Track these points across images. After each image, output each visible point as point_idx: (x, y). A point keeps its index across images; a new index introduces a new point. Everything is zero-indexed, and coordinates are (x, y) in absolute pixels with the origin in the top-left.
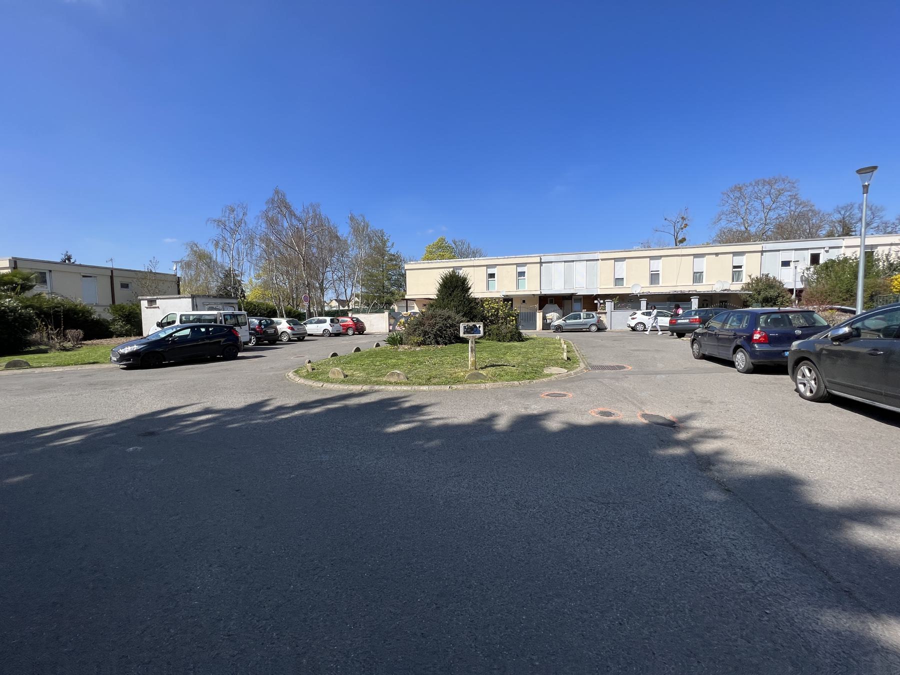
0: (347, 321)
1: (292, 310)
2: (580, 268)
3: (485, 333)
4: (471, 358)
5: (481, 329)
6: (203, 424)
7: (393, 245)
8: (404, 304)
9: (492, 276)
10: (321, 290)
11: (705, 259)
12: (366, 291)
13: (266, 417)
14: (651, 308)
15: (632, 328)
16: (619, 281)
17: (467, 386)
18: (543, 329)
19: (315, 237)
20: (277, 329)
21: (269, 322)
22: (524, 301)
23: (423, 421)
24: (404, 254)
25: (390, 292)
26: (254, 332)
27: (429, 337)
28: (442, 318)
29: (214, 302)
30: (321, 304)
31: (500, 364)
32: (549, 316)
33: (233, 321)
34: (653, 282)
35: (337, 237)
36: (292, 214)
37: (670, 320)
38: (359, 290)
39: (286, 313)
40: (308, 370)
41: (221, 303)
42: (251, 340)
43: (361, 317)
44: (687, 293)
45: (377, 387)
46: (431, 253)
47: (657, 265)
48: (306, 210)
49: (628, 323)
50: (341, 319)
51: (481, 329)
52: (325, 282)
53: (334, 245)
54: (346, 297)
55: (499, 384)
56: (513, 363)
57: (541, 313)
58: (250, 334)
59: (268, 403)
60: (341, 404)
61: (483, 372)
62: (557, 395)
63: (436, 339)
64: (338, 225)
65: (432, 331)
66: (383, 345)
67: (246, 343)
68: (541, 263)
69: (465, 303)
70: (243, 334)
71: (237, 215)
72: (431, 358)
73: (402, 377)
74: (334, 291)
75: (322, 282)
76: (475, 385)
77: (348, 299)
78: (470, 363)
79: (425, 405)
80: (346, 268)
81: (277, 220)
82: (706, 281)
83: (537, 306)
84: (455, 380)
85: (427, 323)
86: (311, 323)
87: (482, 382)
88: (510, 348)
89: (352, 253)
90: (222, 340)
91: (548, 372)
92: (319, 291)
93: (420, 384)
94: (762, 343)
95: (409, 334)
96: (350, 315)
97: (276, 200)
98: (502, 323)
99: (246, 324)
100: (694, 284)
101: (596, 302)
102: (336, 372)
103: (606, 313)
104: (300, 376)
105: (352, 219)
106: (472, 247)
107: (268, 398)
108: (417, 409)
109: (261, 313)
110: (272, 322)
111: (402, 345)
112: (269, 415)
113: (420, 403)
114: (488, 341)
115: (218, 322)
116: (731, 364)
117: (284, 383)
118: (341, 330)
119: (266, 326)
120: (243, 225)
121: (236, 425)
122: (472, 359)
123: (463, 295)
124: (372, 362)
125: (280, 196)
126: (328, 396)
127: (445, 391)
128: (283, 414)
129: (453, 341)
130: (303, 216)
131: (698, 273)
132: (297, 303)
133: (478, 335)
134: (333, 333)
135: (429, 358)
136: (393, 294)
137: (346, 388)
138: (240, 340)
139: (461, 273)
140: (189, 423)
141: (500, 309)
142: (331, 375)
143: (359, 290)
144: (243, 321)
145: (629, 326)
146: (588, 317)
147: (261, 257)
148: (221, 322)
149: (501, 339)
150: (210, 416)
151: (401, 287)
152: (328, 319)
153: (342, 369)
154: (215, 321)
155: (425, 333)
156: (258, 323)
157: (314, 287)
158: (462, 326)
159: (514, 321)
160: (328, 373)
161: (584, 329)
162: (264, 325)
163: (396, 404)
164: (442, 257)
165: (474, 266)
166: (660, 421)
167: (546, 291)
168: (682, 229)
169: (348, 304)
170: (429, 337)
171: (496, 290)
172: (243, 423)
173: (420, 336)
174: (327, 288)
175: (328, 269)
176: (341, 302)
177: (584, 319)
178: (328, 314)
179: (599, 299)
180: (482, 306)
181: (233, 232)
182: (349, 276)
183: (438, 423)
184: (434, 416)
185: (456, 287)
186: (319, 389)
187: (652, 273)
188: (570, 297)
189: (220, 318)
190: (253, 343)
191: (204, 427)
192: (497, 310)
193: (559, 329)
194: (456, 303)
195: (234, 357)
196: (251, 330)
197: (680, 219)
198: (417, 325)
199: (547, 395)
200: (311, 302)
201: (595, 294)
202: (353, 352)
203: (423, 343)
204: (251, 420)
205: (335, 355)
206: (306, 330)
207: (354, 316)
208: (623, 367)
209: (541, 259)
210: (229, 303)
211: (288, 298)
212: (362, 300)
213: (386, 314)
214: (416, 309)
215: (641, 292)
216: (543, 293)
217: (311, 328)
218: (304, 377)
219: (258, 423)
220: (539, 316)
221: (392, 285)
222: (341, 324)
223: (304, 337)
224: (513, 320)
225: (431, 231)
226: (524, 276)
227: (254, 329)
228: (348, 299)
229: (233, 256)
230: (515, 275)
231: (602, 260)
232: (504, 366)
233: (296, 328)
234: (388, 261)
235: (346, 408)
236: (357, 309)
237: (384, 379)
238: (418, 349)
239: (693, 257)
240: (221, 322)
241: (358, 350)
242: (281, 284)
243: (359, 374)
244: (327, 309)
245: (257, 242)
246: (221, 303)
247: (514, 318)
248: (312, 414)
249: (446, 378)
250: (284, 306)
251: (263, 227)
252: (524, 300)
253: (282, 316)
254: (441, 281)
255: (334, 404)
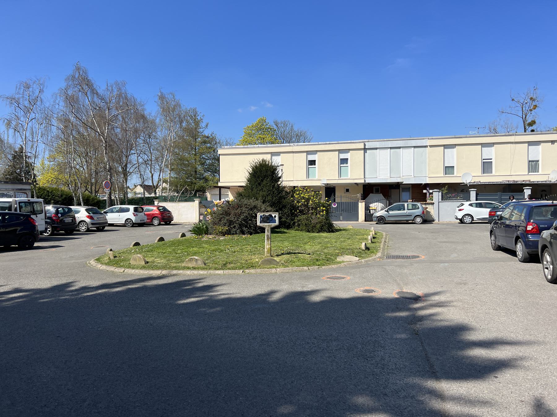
0: (152, 210)
1: (90, 197)
2: (407, 155)
3: (280, 222)
4: (267, 246)
5: (276, 219)
6: (16, 299)
7: (207, 126)
8: (217, 191)
9: (312, 163)
10: (124, 175)
11: (540, 146)
12: (175, 176)
13: (72, 295)
14: (510, 199)
15: (460, 220)
16: (449, 170)
17: (259, 271)
18: (365, 221)
19: (120, 117)
20: (75, 218)
21: (67, 211)
22: (347, 190)
23: (211, 296)
24: (220, 136)
25: (204, 178)
26: (50, 221)
27: (234, 227)
28: (248, 208)
29: (5, 188)
30: (124, 190)
31: (297, 252)
32: (373, 206)
33: (29, 208)
34: (486, 170)
35: (143, 117)
36: (94, 92)
37: (490, 212)
38: (167, 175)
39: (83, 200)
40: (109, 258)
41: (13, 190)
42: (46, 229)
43: (169, 206)
44: (520, 183)
45: (175, 272)
46: (250, 135)
47: (490, 153)
48: (110, 88)
49: (456, 214)
50: (146, 207)
51: (277, 219)
52: (129, 166)
53: (140, 125)
54: (153, 183)
55: (290, 269)
56: (309, 251)
57: (364, 203)
58: (46, 222)
59: (73, 284)
60: (141, 285)
61: (277, 259)
62: (336, 278)
63: (241, 228)
64: (145, 102)
65: (238, 220)
66: (189, 235)
67: (42, 233)
68: (365, 149)
69: (273, 193)
70: (40, 222)
71: (33, 92)
72: (232, 246)
73: (199, 262)
74: (139, 176)
75: (126, 165)
76: (266, 269)
77: (155, 184)
78: (266, 250)
79: (217, 285)
80: (153, 150)
81: (78, 99)
82: (542, 171)
83: (359, 195)
84: (249, 266)
85: (233, 212)
86: (112, 212)
87: (274, 267)
88: (313, 238)
89: (160, 134)
90: (19, 228)
91: (340, 260)
92: (122, 176)
93: (216, 269)
94: (534, 234)
95: (215, 224)
96: (156, 203)
97: (77, 76)
98: (312, 213)
99: (43, 212)
100: (530, 174)
101: (425, 191)
102: (137, 258)
103: (433, 203)
104: (102, 264)
105: (162, 97)
106: (295, 129)
107: (72, 281)
108: (209, 288)
109: (55, 200)
110: (70, 210)
111: (208, 234)
112: (75, 293)
113: (213, 283)
114: (297, 232)
115: (13, 209)
116: (513, 253)
117: (86, 269)
118: (146, 220)
119: (63, 214)
120: (38, 103)
121: (46, 300)
122: (268, 247)
123: (273, 184)
124: (174, 250)
125: (81, 72)
126: (129, 279)
127: (238, 275)
128: (88, 292)
129: (258, 231)
130: (107, 95)
131: (533, 161)
132: (95, 188)
133: (273, 225)
134: (137, 222)
135: (230, 247)
136: (206, 180)
137: (146, 272)
138: (36, 229)
139: (276, 161)
140: (3, 299)
141: (311, 198)
142: (132, 262)
143: (167, 175)
144: (39, 208)
145: (457, 219)
146: (415, 207)
147: (58, 137)
148: (16, 210)
149: (310, 230)
150: (21, 294)
151: (216, 173)
152: (132, 207)
153: (144, 256)
154: (10, 208)
155: (231, 222)
156: (54, 211)
157: (116, 171)
158: (259, 215)
159: (324, 211)
160: (129, 260)
161: (410, 220)
162: (61, 213)
163: (189, 285)
164: (263, 142)
165: (293, 152)
166: (409, 296)
167: (371, 179)
168: (531, 110)
169: (155, 191)
170: (234, 227)
171: (317, 178)
172: (53, 299)
173: (225, 225)
174: (131, 173)
175: (133, 152)
176: (147, 188)
177: (408, 209)
178: (131, 202)
179: (428, 189)
180: (293, 196)
181: (27, 111)
182: (157, 159)
183: (223, 297)
184: (221, 293)
185: (265, 176)
186: (120, 274)
187: (484, 161)
188: (397, 186)
189: (15, 206)
190: (48, 233)
191: (18, 302)
192: (308, 200)
193: (381, 220)
194: (264, 193)
195: (31, 247)
196: (48, 219)
197: (529, 100)
198: (222, 214)
199: (328, 278)
200: (112, 188)
201: (423, 182)
202: (156, 241)
203: (228, 233)
204: (59, 296)
205: (137, 244)
206: (106, 219)
207: (161, 204)
208: (418, 257)
209: (365, 145)
210: (21, 189)
211: (86, 182)
212: (170, 186)
213: (197, 202)
214: (231, 197)
215: (473, 181)
216: (368, 181)
217: (112, 217)
218: (106, 264)
219: (66, 298)
220: (362, 206)
221: (207, 170)
222: (146, 213)
223: (104, 227)
224: (323, 210)
225: (253, 108)
226: (347, 163)
227: (49, 218)
228: (155, 184)
229: (26, 136)
230: (336, 162)
231: (431, 146)
232: (300, 253)
233: (96, 217)
234: (202, 143)
235: (145, 287)
236: (164, 196)
237: (183, 265)
238: (222, 238)
239: (527, 144)
240: (16, 210)
241: (161, 239)
242: (78, 167)
243: (160, 261)
244: (130, 196)
245: (54, 122)
246: (13, 190)
247: (324, 208)
248: (114, 292)
249: (241, 263)
250: (81, 192)
251: (61, 106)
252: (347, 189)
253: (79, 204)
254: (251, 169)
255: (133, 285)
